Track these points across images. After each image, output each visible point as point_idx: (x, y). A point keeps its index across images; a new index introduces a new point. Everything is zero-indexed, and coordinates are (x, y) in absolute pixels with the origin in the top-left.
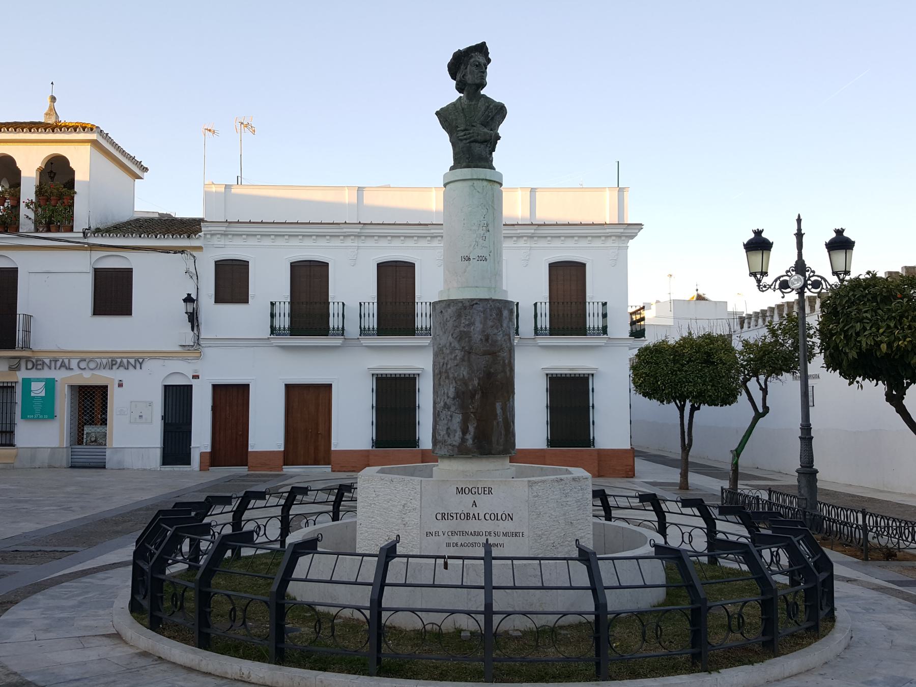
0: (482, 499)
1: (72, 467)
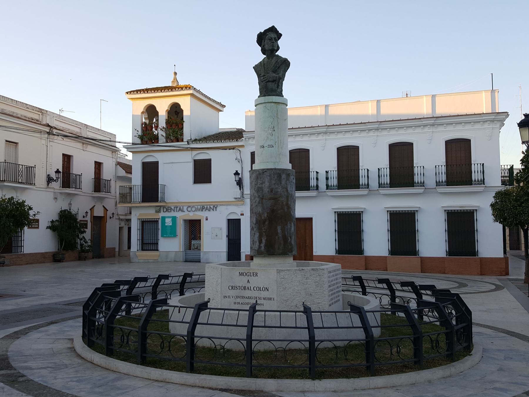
0: (252, 279)
1: (186, 261)
